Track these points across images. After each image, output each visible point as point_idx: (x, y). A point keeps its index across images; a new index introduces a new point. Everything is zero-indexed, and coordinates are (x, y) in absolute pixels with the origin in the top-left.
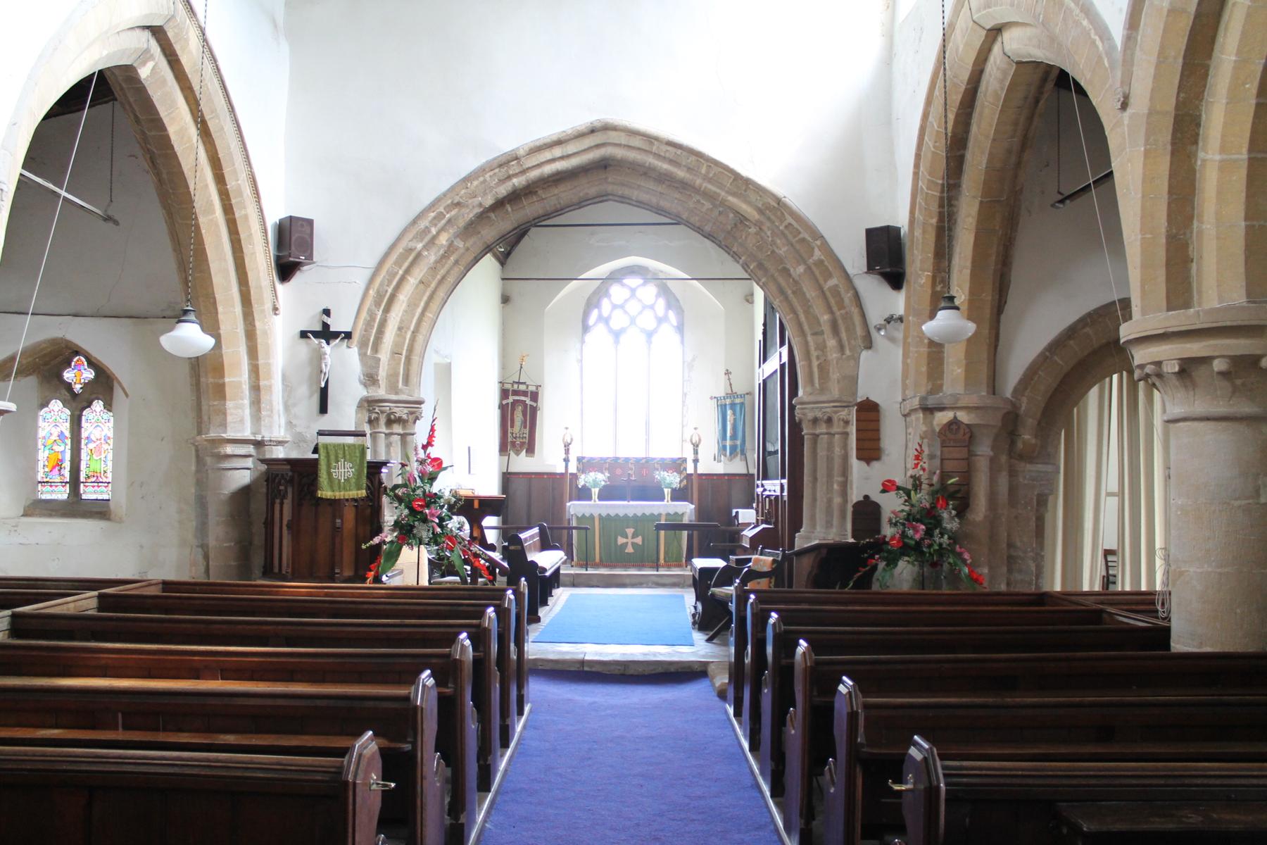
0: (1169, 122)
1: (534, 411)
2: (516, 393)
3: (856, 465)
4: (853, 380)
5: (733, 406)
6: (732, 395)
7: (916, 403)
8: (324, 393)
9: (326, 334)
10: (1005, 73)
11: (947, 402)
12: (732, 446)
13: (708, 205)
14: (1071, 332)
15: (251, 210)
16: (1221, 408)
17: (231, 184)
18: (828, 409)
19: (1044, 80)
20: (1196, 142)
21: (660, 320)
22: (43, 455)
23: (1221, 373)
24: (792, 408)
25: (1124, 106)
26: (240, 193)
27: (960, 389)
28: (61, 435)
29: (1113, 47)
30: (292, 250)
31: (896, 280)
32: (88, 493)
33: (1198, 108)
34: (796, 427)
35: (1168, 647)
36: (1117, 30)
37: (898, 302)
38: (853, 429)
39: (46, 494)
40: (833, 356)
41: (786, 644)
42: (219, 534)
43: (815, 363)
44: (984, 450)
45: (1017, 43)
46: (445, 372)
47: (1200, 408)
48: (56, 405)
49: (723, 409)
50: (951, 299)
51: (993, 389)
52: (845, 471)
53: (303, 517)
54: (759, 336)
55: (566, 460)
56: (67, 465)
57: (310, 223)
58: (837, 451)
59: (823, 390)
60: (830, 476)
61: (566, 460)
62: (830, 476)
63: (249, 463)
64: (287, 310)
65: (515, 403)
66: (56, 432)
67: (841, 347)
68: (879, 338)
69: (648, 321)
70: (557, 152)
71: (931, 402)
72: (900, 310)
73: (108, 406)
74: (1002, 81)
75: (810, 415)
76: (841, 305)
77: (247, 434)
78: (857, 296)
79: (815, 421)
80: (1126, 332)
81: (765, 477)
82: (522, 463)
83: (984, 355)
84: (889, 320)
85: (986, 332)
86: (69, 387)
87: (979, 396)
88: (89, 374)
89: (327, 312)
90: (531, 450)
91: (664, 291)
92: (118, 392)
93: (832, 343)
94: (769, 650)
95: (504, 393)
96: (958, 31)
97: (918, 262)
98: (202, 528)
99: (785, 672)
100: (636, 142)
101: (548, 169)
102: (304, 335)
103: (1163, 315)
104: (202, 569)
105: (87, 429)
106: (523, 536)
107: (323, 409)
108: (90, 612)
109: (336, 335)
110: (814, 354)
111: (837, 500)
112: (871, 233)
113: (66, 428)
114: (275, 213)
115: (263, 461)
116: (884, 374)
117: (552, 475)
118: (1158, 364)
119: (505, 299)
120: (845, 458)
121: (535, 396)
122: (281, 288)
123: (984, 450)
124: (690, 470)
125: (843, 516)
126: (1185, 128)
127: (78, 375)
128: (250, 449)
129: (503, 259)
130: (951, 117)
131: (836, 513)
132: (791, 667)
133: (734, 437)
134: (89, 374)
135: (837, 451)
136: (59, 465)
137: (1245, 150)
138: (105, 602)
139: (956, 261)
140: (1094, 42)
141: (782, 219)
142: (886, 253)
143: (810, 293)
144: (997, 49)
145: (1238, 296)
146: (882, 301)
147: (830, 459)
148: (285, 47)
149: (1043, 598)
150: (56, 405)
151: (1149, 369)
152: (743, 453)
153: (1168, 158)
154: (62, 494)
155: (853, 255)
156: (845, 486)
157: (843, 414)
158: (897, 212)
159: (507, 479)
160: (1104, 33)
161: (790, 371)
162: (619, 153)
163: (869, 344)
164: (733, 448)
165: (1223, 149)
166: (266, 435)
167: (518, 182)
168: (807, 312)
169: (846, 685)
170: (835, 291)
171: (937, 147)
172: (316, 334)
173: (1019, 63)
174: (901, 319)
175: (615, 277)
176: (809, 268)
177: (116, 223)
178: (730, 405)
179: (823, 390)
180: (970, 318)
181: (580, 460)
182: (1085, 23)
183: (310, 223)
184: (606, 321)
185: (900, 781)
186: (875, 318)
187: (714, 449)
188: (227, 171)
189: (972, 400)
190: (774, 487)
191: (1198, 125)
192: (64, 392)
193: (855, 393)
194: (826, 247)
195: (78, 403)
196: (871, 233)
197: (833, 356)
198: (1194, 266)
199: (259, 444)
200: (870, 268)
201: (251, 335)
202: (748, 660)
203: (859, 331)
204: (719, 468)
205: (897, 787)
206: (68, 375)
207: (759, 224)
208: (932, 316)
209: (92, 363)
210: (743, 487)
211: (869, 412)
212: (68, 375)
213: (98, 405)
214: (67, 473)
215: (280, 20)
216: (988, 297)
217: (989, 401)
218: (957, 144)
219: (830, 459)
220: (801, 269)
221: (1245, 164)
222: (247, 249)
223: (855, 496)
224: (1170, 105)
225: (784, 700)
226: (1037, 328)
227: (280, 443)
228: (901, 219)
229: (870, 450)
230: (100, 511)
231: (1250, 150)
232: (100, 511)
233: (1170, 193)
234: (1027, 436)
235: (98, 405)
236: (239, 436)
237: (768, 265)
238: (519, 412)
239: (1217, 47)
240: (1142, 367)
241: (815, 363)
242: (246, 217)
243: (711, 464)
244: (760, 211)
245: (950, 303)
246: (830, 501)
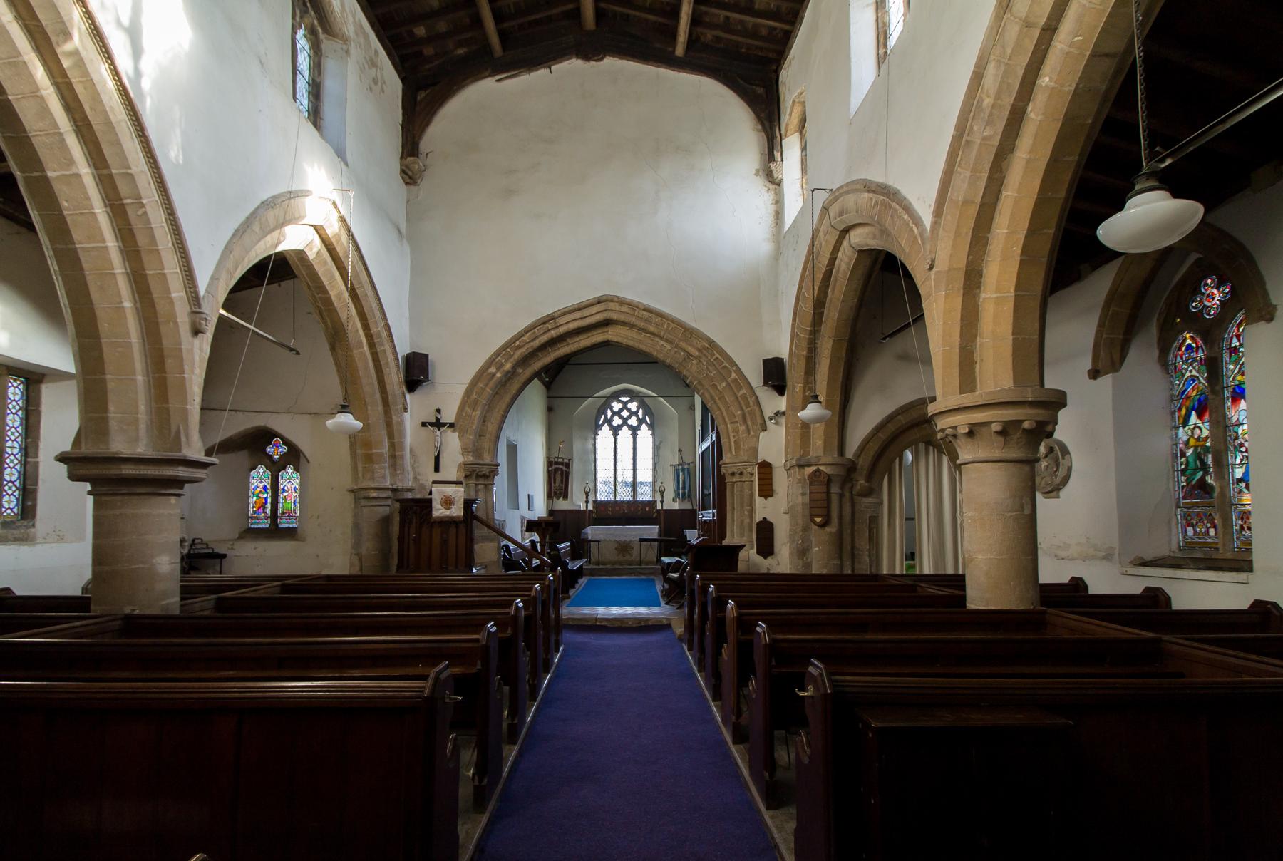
0: (962, 275)
1: (567, 474)
2: (557, 463)
3: (759, 501)
4: (756, 450)
5: (683, 470)
6: (682, 463)
7: (794, 462)
8: (437, 459)
9: (438, 424)
10: (850, 259)
11: (813, 461)
12: (684, 493)
13: (668, 347)
14: (890, 419)
15: (387, 347)
16: (998, 454)
17: (374, 330)
18: (740, 467)
19: (875, 262)
20: (979, 287)
21: (641, 422)
22: (253, 500)
23: (998, 433)
24: (719, 467)
25: (931, 268)
26: (379, 336)
27: (820, 453)
28: (265, 488)
29: (925, 230)
30: (417, 371)
31: (781, 390)
32: (283, 523)
33: (980, 265)
34: (722, 478)
35: (965, 606)
36: (927, 220)
37: (782, 403)
38: (756, 478)
39: (255, 525)
40: (743, 435)
41: (720, 604)
42: (368, 546)
43: (732, 440)
44: (835, 489)
45: (859, 238)
46: (513, 450)
47: (982, 454)
48: (261, 469)
49: (677, 472)
50: (817, 397)
51: (841, 451)
52: (751, 503)
53: (419, 537)
54: (698, 427)
55: (587, 502)
56: (269, 506)
57: (426, 356)
58: (747, 491)
59: (737, 455)
60: (742, 506)
61: (587, 502)
62: (742, 506)
63: (389, 502)
64: (416, 408)
65: (556, 470)
66: (261, 485)
67: (748, 430)
68: (770, 424)
69: (633, 421)
70: (577, 315)
71: (802, 462)
72: (783, 408)
73: (297, 470)
74: (848, 264)
75: (731, 471)
76: (748, 405)
77: (388, 484)
78: (757, 401)
79: (733, 474)
80: (932, 409)
81: (704, 509)
82: (562, 505)
83: (836, 434)
84: (777, 414)
85: (836, 419)
86: (270, 457)
87: (833, 457)
88: (284, 449)
89: (438, 411)
90: (565, 497)
91: (642, 404)
92: (302, 460)
93: (743, 428)
94: (710, 610)
95: (550, 463)
96: (821, 234)
97: (795, 378)
98: (357, 544)
99: (720, 622)
100: (625, 309)
101: (572, 326)
102: (424, 424)
103: (958, 396)
104: (358, 568)
105: (283, 483)
106: (560, 546)
107: (437, 469)
108: (206, 613)
109: (444, 425)
110: (732, 434)
111: (747, 520)
112: (766, 362)
113: (268, 483)
114: (403, 349)
115: (397, 501)
116: (773, 445)
117: (579, 511)
118: (955, 428)
119: (550, 409)
120: (752, 496)
121: (567, 465)
122: (408, 396)
123: (835, 489)
124: (659, 507)
125: (751, 530)
126: (972, 279)
127: (276, 450)
128: (389, 494)
129: (548, 386)
130: (816, 288)
131: (746, 529)
132: (724, 618)
133: (684, 488)
134: (284, 449)
135: (747, 491)
136: (264, 506)
137: (1012, 290)
138: (221, 605)
139: (818, 377)
140: (911, 229)
141: (712, 355)
142: (775, 373)
143: (729, 398)
144: (845, 243)
145: (1006, 382)
146: (773, 403)
147: (742, 497)
148: (407, 248)
149: (876, 577)
150: (261, 469)
151: (949, 431)
152: (690, 496)
153: (961, 298)
154: (265, 524)
155: (755, 376)
156: (752, 512)
157: (750, 469)
158: (781, 347)
159: (551, 512)
160: (917, 220)
161: (718, 445)
162: (615, 316)
163: (764, 428)
164: (684, 494)
165: (998, 290)
166: (400, 485)
167: (554, 333)
168: (728, 408)
169: (761, 627)
170: (744, 396)
171: (808, 308)
172: (432, 424)
173: (860, 251)
174: (784, 413)
175: (615, 396)
176: (728, 384)
177: (298, 353)
178: (682, 469)
179: (737, 455)
180: (826, 408)
181: (595, 502)
182: (906, 217)
183: (426, 356)
184: (609, 422)
185: (803, 690)
186: (768, 412)
187: (673, 495)
188: (370, 322)
189: (829, 460)
190: (708, 515)
191: (981, 276)
192: (268, 462)
193: (756, 457)
194: (739, 371)
195: (276, 468)
196: (766, 362)
197: (743, 435)
198: (977, 366)
199: (394, 490)
200: (766, 384)
201: (389, 424)
202: (696, 616)
203: (759, 421)
204: (676, 506)
205: (801, 694)
206: (270, 450)
207: (698, 358)
208: (804, 408)
209: (286, 442)
210: (688, 518)
211: (766, 468)
212: (270, 450)
213: (290, 470)
214: (268, 511)
215: (403, 227)
216: (837, 398)
217: (838, 460)
218: (819, 305)
219: (742, 497)
220: (724, 384)
221: (1012, 300)
222: (386, 371)
223: (758, 518)
224: (962, 264)
225: (720, 638)
226: (868, 417)
227: (409, 490)
228: (784, 353)
229: (767, 490)
230: (291, 533)
231: (1016, 290)
232: (291, 533)
233: (962, 320)
234: (861, 482)
235: (290, 470)
236: (382, 485)
237: (704, 382)
238: (558, 477)
239: (994, 225)
240: (943, 430)
241: (732, 440)
242: (384, 351)
243: (671, 503)
244: (699, 350)
245: (815, 399)
246: (742, 522)
